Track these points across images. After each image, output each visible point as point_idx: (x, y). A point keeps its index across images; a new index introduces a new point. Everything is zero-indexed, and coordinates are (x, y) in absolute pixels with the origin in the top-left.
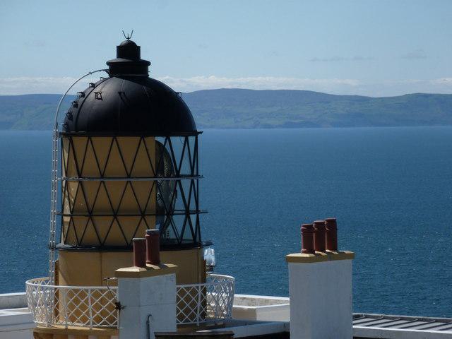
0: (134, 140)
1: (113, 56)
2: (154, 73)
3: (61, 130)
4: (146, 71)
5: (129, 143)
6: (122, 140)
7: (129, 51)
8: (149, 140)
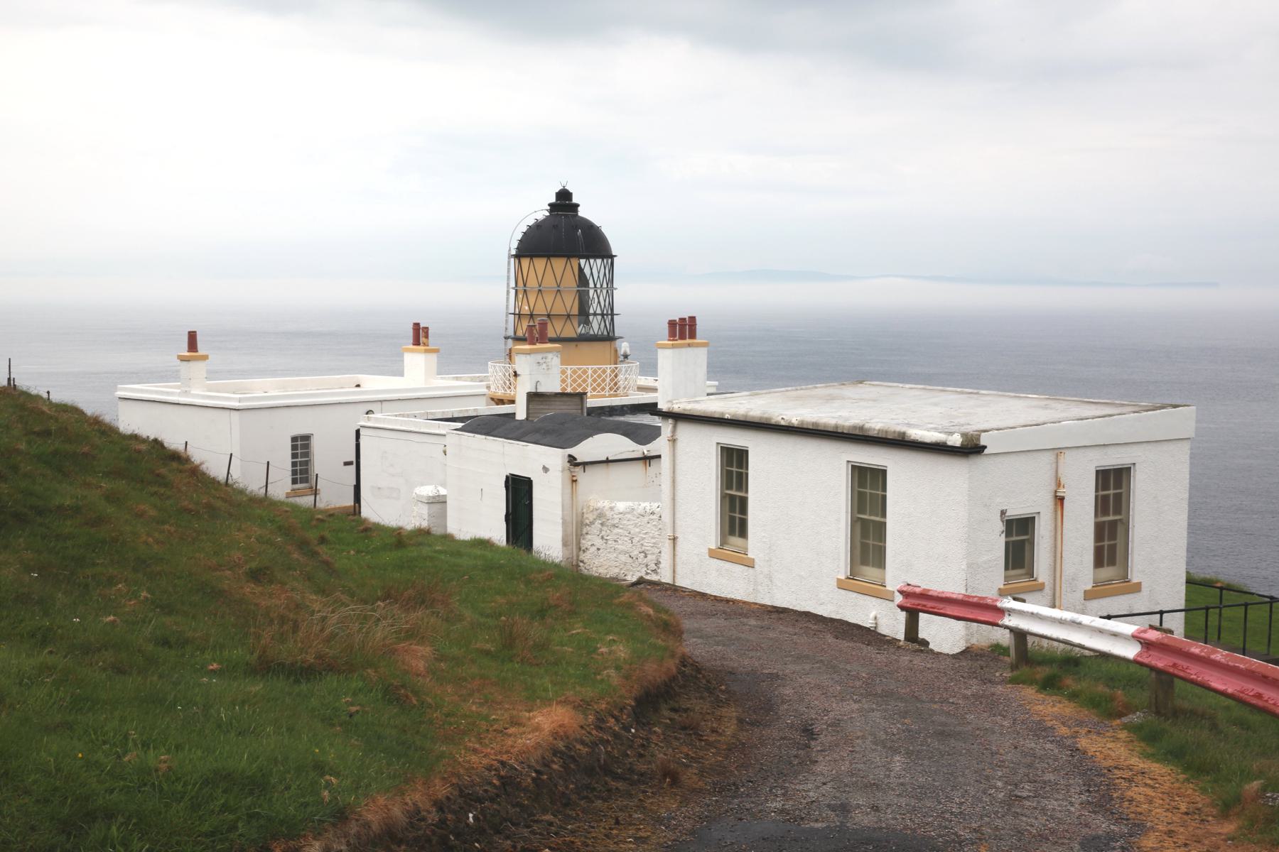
0: (563, 260)
1: (553, 200)
2: (582, 212)
3: (514, 252)
4: (576, 211)
5: (559, 263)
6: (554, 260)
7: (564, 195)
8: (574, 262)
